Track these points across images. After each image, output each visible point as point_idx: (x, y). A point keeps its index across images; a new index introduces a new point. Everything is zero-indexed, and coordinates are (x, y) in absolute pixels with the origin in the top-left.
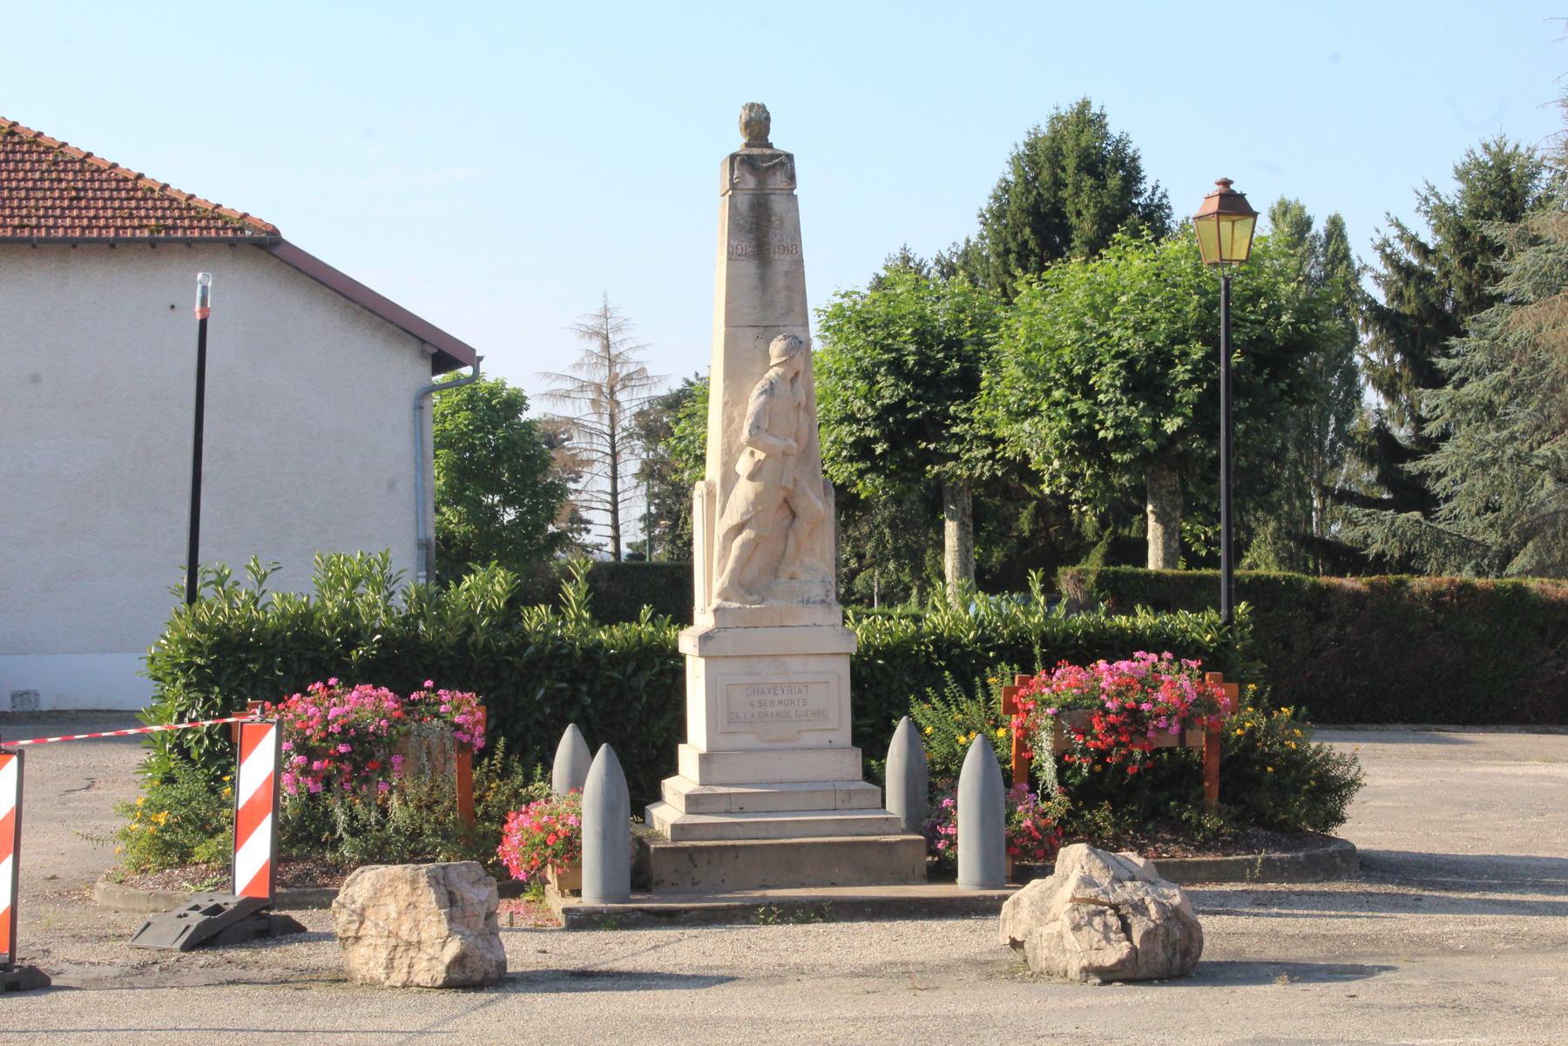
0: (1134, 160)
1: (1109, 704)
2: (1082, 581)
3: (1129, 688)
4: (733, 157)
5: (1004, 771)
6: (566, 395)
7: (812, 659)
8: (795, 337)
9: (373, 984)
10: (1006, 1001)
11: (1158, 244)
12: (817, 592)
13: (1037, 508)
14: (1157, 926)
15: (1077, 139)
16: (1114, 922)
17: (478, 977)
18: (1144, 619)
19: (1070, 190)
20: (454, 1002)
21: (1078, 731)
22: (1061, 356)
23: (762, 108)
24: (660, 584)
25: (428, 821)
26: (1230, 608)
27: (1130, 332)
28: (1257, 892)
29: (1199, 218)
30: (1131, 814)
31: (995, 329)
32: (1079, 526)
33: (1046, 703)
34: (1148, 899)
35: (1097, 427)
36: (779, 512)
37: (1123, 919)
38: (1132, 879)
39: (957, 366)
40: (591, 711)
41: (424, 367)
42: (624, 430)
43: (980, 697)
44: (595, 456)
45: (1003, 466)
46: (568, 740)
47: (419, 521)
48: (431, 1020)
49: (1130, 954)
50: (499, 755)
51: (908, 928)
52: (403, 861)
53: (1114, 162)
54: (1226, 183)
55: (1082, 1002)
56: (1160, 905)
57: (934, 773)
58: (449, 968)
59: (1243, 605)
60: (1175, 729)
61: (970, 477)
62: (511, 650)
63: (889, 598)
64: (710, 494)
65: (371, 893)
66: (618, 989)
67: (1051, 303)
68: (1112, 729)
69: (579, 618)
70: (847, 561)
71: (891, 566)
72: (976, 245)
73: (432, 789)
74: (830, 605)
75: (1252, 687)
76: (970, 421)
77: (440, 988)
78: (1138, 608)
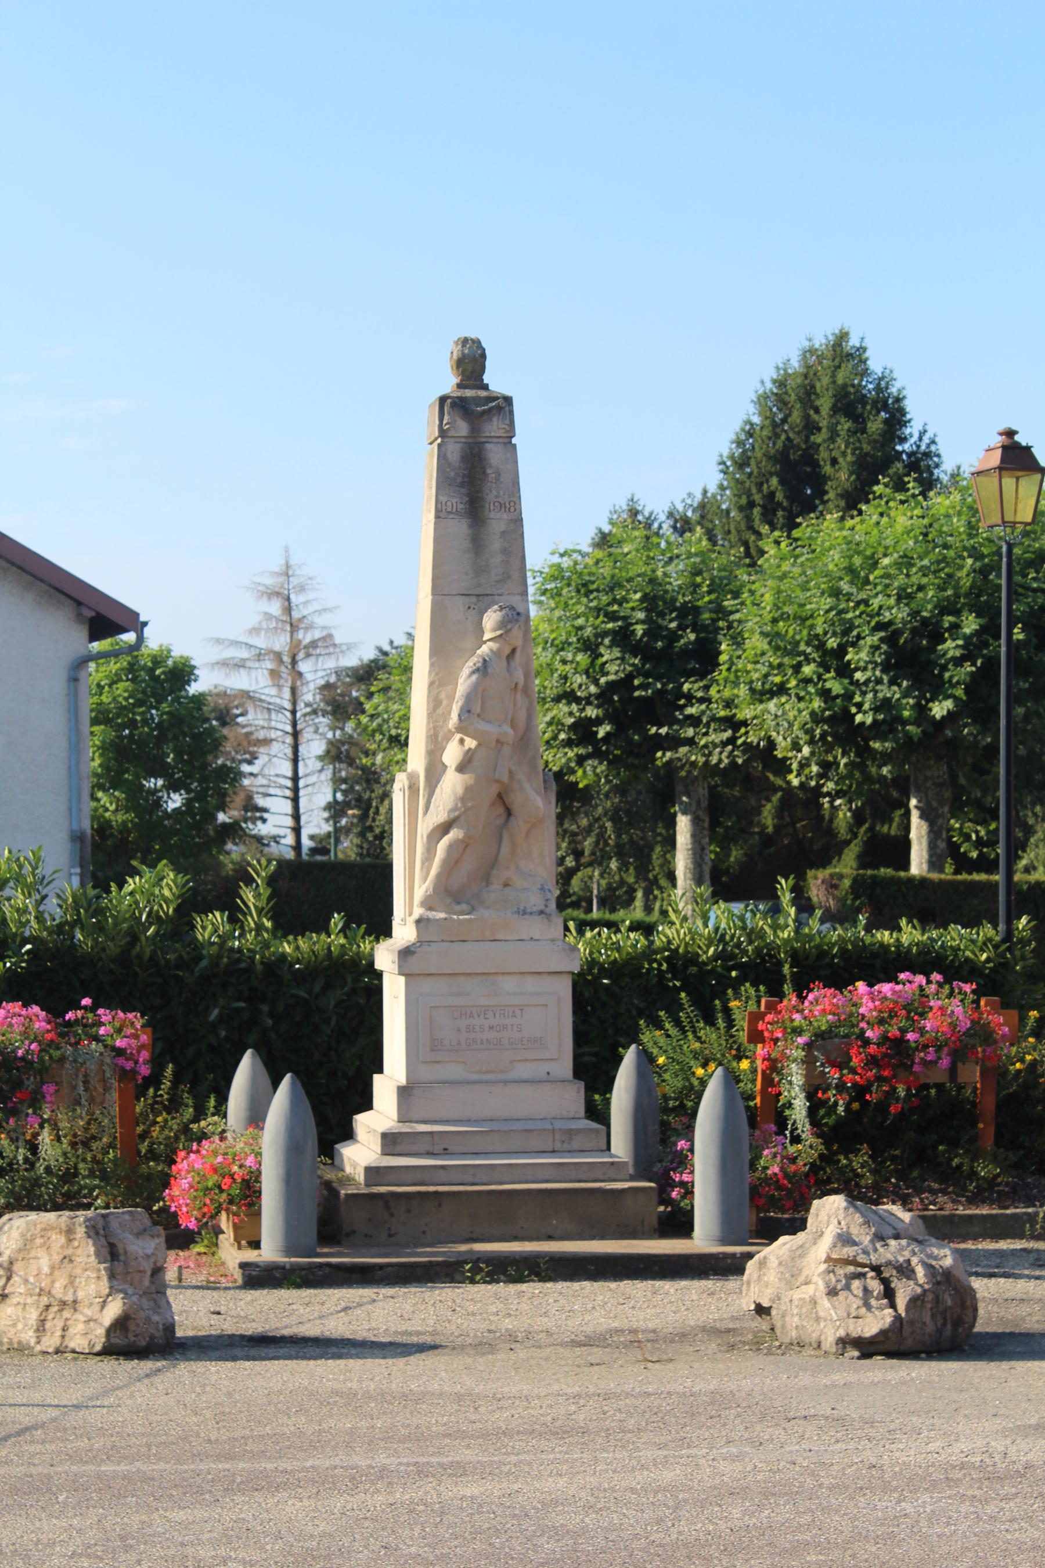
0: (898, 400)
1: (869, 1034)
2: (835, 887)
3: (893, 1013)
4: (443, 400)
5: (748, 1108)
6: (240, 665)
7: (529, 979)
8: (512, 608)
9: (21, 1349)
10: (749, 1376)
11: (925, 498)
12: (535, 901)
13: (782, 800)
14: (925, 1291)
15: (833, 375)
16: (876, 1286)
17: (143, 1342)
18: (909, 934)
19: (824, 434)
20: (114, 1371)
21: (833, 1064)
22: (812, 627)
23: (477, 343)
24: (358, 888)
25: (84, 1160)
26: (1009, 922)
27: (892, 601)
28: (1038, 1251)
29: (979, 473)
30: (894, 1159)
31: (736, 595)
32: (831, 821)
33: (798, 1031)
34: (914, 1261)
35: (854, 710)
36: (491, 810)
37: (886, 1282)
38: (897, 1237)
39: (692, 637)
40: (273, 1035)
41: (81, 633)
42: (307, 705)
43: (721, 1023)
44: (273, 735)
45: (744, 752)
46: (246, 1070)
47: (73, 810)
48: (89, 1392)
49: (893, 1323)
50: (166, 1084)
51: (637, 1289)
52: (56, 1208)
53: (875, 402)
54: (1010, 433)
55: (838, 1378)
56: (928, 1267)
57: (666, 1110)
58: (109, 1332)
59: (1024, 920)
60: (945, 1062)
61: (706, 763)
63: (609, 901)
64: (413, 788)
65: (20, 1244)
66: (303, 1358)
67: (802, 565)
68: (872, 1061)
69: (259, 928)
71: (614, 865)
72: (714, 496)
73: (89, 1123)
74: (549, 916)
75: (1034, 1014)
76: (708, 700)
77: (98, 1354)
78: (903, 922)
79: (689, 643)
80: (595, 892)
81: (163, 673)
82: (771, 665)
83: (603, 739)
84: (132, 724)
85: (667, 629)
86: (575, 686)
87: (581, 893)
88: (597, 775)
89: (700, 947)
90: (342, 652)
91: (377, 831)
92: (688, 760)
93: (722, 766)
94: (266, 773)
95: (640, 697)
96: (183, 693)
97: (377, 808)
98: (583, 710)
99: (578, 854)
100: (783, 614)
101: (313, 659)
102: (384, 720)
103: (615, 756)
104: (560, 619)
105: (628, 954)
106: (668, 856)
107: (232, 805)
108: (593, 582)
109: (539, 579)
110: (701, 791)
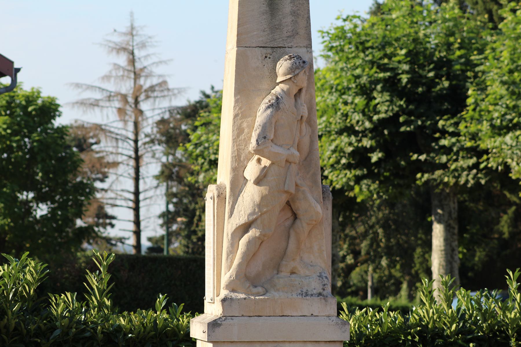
6: (95, 104)
8: (299, 57)
12: (315, 286)
31: (481, 51)
36: (282, 214)
39: (446, 84)
42: (147, 136)
44: (120, 159)
45: (486, 175)
61: (456, 184)
62: (39, 332)
63: (381, 291)
64: (221, 196)
69: (101, 305)
70: (344, 257)
71: (384, 262)
74: (325, 297)
79: (444, 89)
80: (370, 283)
81: (34, 110)
82: (507, 107)
83: (376, 163)
84: (9, 149)
85: (426, 77)
86: (354, 122)
87: (359, 285)
88: (370, 192)
89: (445, 324)
90: (174, 95)
91: (200, 234)
92: (442, 181)
93: (469, 185)
94: (114, 188)
95: (406, 132)
96: (50, 126)
97: (200, 217)
98: (360, 141)
99: (356, 254)
100: (517, 66)
101: (151, 100)
102: (205, 148)
103: (385, 177)
104: (342, 69)
105: (389, 328)
106: (427, 256)
107: (88, 213)
108: (368, 41)
109: (327, 39)
110: (452, 205)
